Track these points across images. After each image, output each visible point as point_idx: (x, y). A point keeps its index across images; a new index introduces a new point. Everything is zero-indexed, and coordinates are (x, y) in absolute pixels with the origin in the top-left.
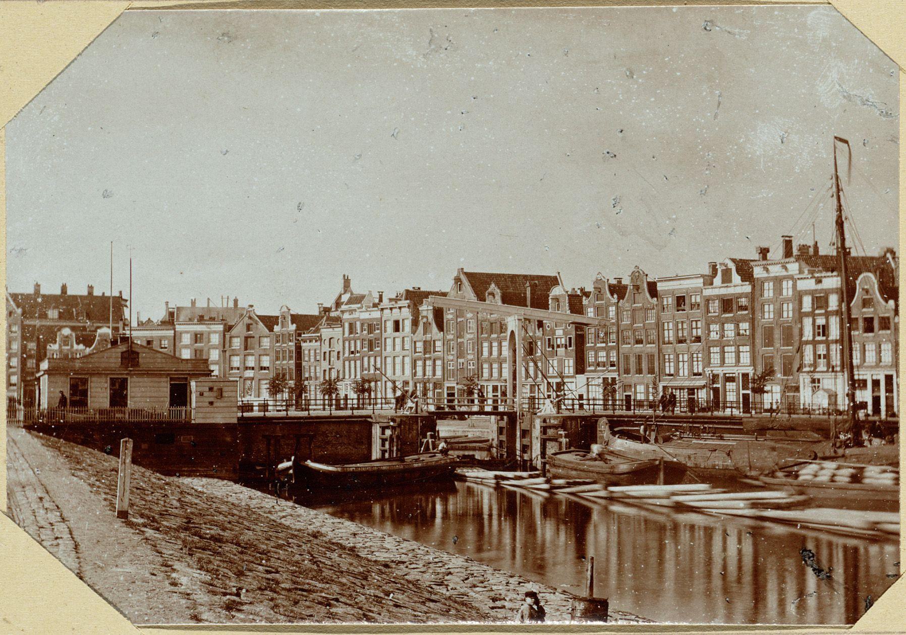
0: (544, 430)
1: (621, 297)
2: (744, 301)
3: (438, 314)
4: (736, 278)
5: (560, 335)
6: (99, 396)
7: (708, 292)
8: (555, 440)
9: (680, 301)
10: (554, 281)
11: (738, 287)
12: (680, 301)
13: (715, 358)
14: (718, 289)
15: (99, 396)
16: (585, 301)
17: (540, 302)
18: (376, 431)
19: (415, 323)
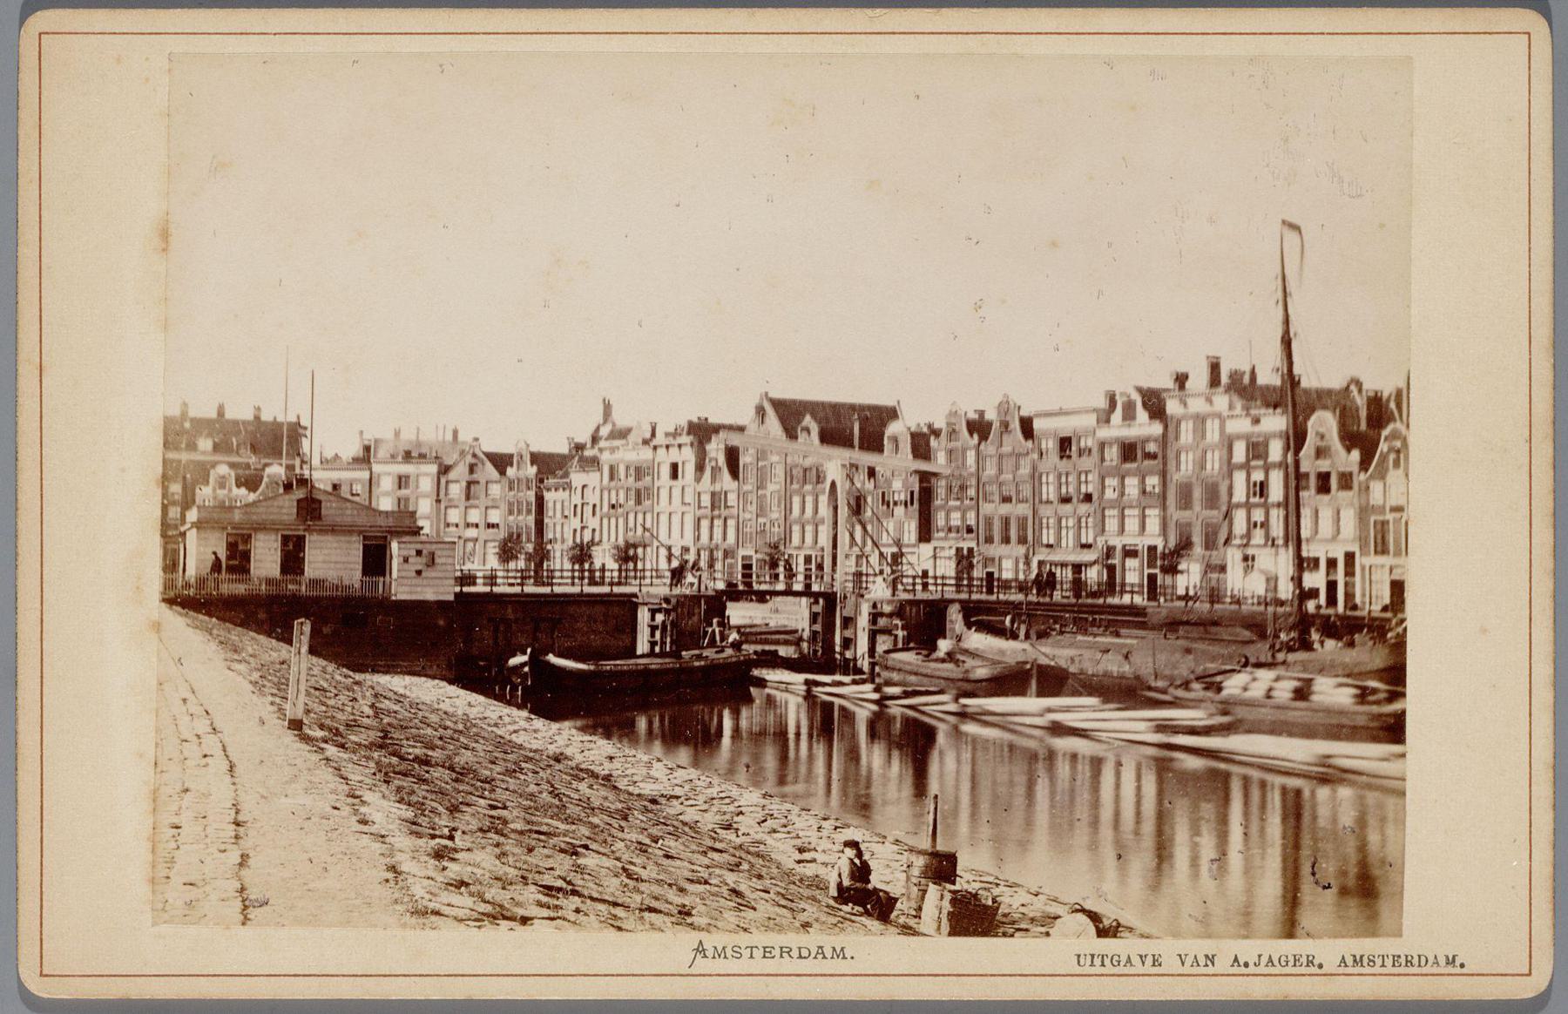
0: (875, 617)
1: (984, 437)
2: (1152, 447)
3: (732, 456)
4: (1142, 415)
5: (899, 488)
6: (266, 559)
7: (1104, 433)
8: (887, 631)
9: (1065, 444)
10: (892, 414)
11: (1144, 427)
12: (1065, 444)
13: (1112, 524)
14: (1117, 429)
15: (266, 559)
16: (933, 442)
17: (873, 442)
18: (643, 615)
19: (700, 468)
